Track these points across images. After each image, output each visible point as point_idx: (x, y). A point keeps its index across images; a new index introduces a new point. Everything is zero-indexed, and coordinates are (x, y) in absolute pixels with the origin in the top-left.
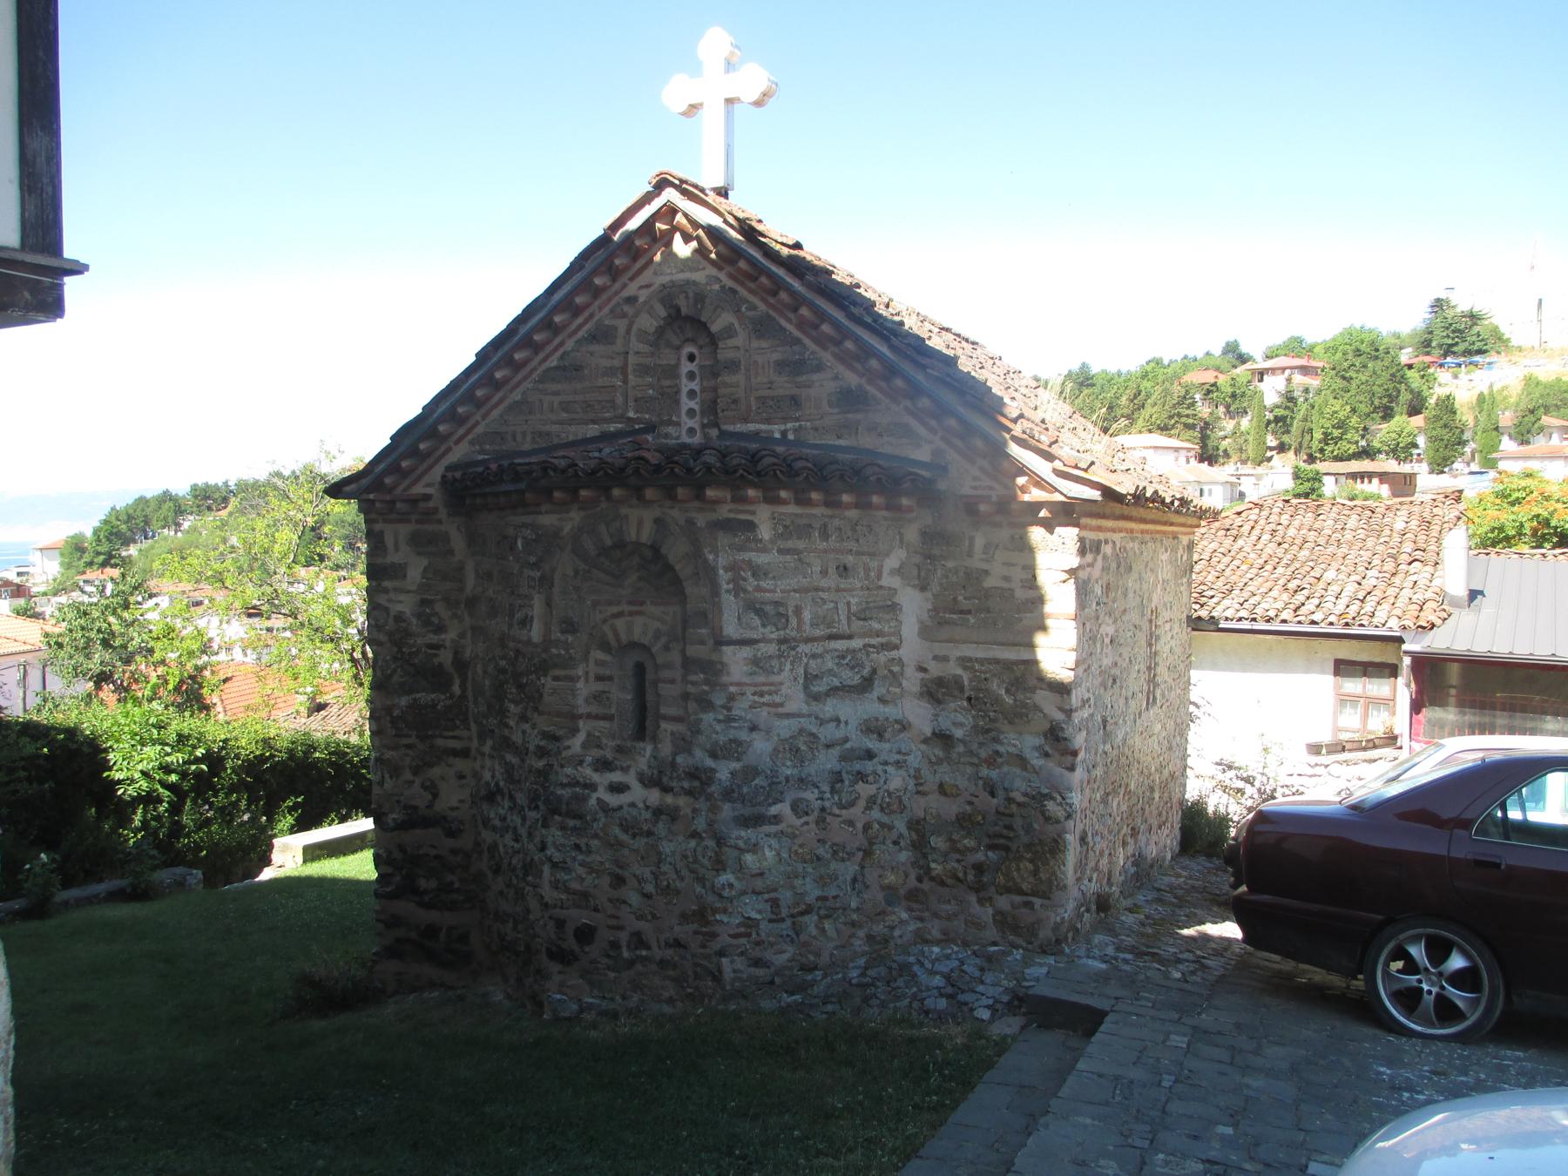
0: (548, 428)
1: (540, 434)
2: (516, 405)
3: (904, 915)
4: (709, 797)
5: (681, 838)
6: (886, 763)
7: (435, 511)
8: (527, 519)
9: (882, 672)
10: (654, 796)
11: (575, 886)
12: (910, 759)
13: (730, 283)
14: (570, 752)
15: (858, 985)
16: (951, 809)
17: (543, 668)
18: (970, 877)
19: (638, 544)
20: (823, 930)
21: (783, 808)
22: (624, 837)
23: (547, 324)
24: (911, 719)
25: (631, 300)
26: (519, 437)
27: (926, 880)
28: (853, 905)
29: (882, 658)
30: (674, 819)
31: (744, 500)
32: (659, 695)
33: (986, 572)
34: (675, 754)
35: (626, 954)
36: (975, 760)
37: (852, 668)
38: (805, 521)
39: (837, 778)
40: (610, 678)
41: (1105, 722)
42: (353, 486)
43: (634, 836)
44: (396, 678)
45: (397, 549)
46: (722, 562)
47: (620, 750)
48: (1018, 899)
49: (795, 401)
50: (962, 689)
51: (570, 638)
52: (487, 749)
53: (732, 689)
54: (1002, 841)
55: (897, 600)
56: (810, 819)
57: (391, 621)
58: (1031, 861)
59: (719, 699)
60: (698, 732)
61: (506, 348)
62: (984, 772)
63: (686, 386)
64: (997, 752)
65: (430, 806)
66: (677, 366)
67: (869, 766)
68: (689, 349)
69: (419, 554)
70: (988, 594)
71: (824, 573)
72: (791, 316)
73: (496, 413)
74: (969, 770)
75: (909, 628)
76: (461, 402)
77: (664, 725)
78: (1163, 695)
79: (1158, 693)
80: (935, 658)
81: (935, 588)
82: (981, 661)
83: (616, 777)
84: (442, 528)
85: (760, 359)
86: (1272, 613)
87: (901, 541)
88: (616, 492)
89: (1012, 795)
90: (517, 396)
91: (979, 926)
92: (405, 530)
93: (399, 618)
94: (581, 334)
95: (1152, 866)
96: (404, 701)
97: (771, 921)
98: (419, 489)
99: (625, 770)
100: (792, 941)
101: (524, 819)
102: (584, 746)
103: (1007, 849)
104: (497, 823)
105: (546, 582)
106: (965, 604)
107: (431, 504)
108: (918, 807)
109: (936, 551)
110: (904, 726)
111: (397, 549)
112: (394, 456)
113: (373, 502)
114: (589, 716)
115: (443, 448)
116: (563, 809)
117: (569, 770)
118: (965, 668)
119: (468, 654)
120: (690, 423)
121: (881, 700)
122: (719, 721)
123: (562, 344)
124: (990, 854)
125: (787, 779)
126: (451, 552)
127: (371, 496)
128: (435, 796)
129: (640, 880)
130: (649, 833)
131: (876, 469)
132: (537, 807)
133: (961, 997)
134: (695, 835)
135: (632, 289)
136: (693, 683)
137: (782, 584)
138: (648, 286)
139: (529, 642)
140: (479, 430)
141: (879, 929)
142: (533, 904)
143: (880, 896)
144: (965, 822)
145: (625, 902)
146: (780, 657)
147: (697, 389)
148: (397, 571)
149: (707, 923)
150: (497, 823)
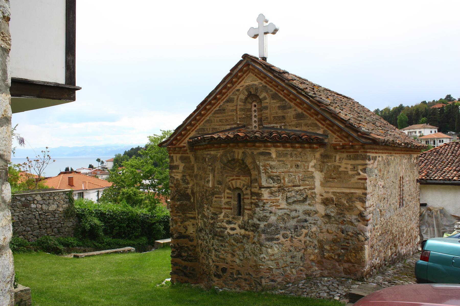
0: (216, 127)
1: (214, 129)
2: (208, 120)
3: (317, 268)
4: (258, 232)
5: (250, 244)
6: (311, 223)
8: (209, 152)
9: (309, 196)
10: (243, 231)
11: (221, 256)
12: (318, 222)
13: (265, 84)
14: (220, 218)
15: (301, 288)
16: (330, 237)
17: (213, 194)
18: (336, 258)
19: (238, 159)
20: (292, 272)
21: (280, 236)
22: (234, 243)
23: (215, 98)
24: (318, 210)
25: (238, 90)
26: (208, 130)
29: (309, 192)
30: (248, 238)
31: (267, 147)
32: (244, 203)
33: (340, 166)
34: (248, 220)
35: (235, 277)
36: (338, 223)
37: (300, 195)
38: (286, 152)
39: (296, 227)
40: (231, 198)
42: (165, 144)
43: (237, 243)
44: (176, 197)
45: (177, 161)
46: (261, 164)
47: (233, 218)
48: (350, 265)
49: (284, 117)
50: (333, 201)
51: (220, 186)
52: (199, 217)
53: (265, 201)
55: (313, 175)
56: (288, 239)
57: (175, 181)
58: (354, 253)
59: (261, 204)
60: (255, 213)
61: (204, 105)
62: (340, 226)
63: (254, 114)
64: (344, 220)
66: (251, 108)
67: (305, 224)
68: (254, 103)
71: (291, 167)
72: (282, 93)
73: (202, 123)
74: (336, 226)
75: (318, 183)
76: (192, 120)
77: (246, 211)
78: (407, 203)
79: (404, 202)
80: (325, 192)
81: (325, 171)
82: (339, 193)
83: (232, 226)
84: (188, 155)
85: (274, 106)
86: (450, 178)
87: (315, 158)
88: (231, 144)
89: (349, 233)
90: (208, 118)
91: (339, 272)
92: (179, 155)
94: (224, 100)
95: (404, 256)
96: (178, 203)
97: (276, 269)
98: (182, 144)
99: (235, 224)
100: (283, 275)
101: (208, 237)
102: (224, 217)
103: (347, 249)
104: (202, 238)
105: (213, 170)
106: (334, 176)
107: (185, 149)
108: (321, 237)
109: (325, 161)
110: (316, 212)
111: (177, 161)
112: (175, 135)
114: (225, 208)
115: (189, 133)
116: (218, 235)
117: (219, 224)
118: (334, 195)
120: (255, 125)
121: (309, 204)
122: (261, 210)
123: (220, 103)
124: (342, 251)
125: (281, 227)
126: (191, 162)
128: (187, 230)
130: (242, 242)
131: (306, 136)
133: (331, 293)
134: (254, 243)
135: (238, 87)
136: (254, 199)
138: (242, 86)
139: (209, 187)
140: (198, 128)
141: (309, 272)
144: (335, 241)
145: (235, 262)
146: (279, 192)
147: (257, 115)
150: (202, 238)
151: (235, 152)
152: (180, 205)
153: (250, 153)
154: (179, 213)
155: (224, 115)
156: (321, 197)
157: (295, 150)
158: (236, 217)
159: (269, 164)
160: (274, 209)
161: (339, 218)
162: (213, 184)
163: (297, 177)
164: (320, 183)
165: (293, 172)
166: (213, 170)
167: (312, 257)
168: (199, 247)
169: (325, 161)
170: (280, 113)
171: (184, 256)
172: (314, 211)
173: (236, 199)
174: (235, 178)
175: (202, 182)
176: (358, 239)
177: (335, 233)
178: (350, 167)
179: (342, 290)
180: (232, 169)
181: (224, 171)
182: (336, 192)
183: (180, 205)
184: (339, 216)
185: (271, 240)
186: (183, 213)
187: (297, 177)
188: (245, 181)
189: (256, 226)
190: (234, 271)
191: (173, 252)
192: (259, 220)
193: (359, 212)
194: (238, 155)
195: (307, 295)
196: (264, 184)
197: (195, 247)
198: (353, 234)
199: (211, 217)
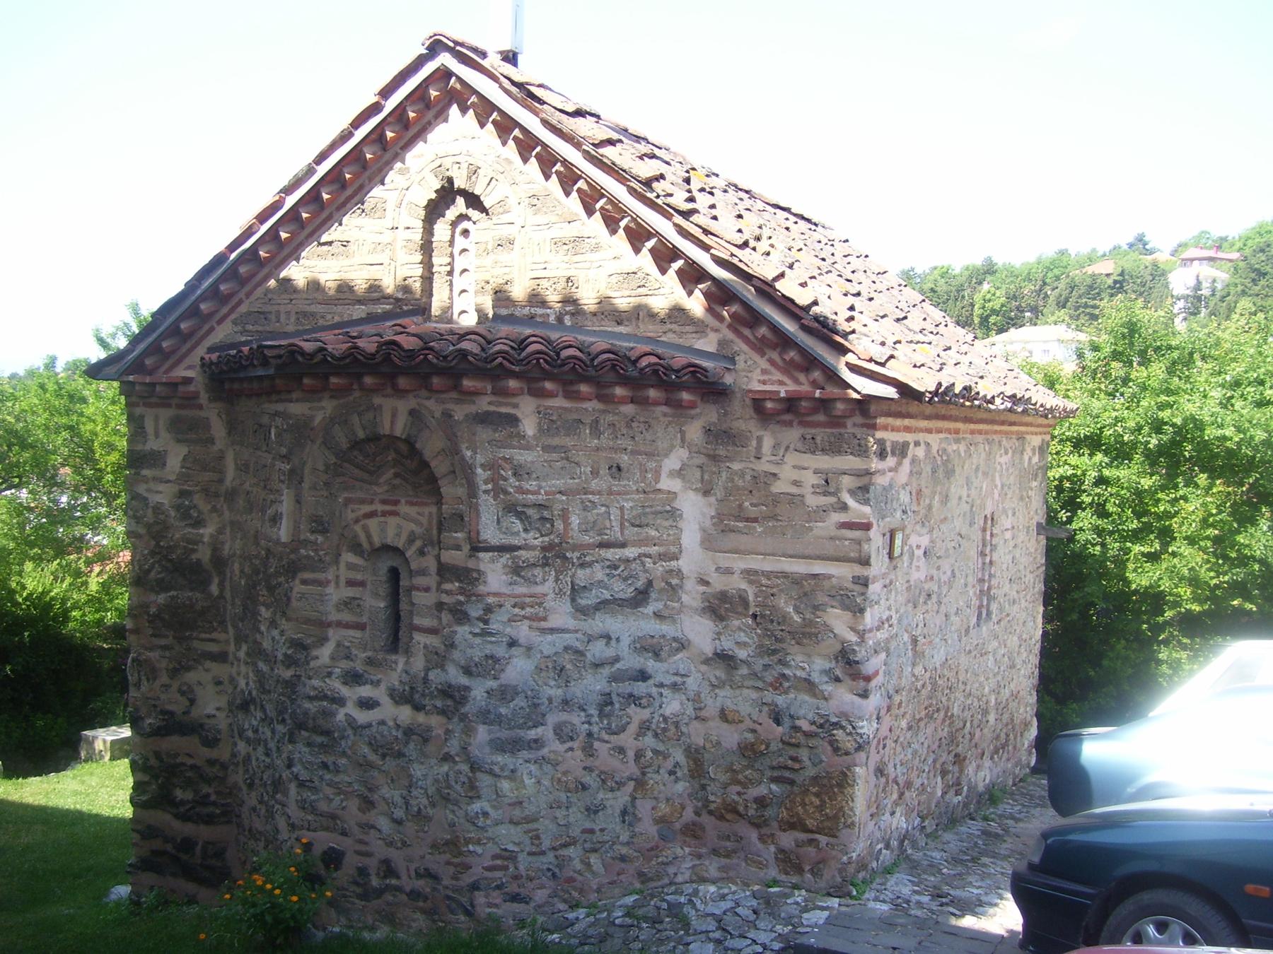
0: (313, 308)
1: (305, 314)
4: (464, 717)
5: (433, 761)
6: (661, 685)
7: (195, 396)
8: (280, 407)
9: (659, 584)
10: (405, 714)
12: (689, 681)
17: (292, 570)
19: (393, 438)
20: (588, 865)
22: (372, 757)
24: (691, 636)
27: (704, 813)
28: (624, 837)
29: (660, 568)
30: (426, 740)
32: (413, 604)
34: (427, 670)
35: (375, 882)
36: (760, 684)
37: (625, 579)
38: (575, 416)
39: (606, 701)
40: (362, 584)
41: (915, 641)
45: (157, 435)
46: (480, 459)
47: (370, 662)
50: (744, 602)
51: (320, 539)
52: (242, 654)
53: (490, 600)
54: (787, 774)
56: (575, 744)
58: (817, 795)
59: (475, 611)
60: (452, 646)
62: (769, 696)
65: (186, 713)
67: (640, 688)
69: (179, 441)
70: (776, 500)
71: (595, 473)
74: (754, 695)
75: (690, 537)
77: (419, 638)
78: (1001, 609)
81: (719, 493)
83: (365, 691)
84: (203, 414)
87: (683, 440)
88: (368, 380)
89: (798, 723)
92: (166, 414)
93: (157, 509)
96: (161, 598)
97: (530, 854)
98: (181, 372)
99: (376, 684)
101: (273, 731)
104: (250, 734)
105: (295, 477)
106: (753, 511)
107: (192, 388)
109: (721, 451)
110: (682, 645)
111: (157, 435)
113: (132, 383)
114: (339, 624)
115: (206, 327)
116: (317, 729)
117: (316, 682)
118: (751, 582)
119: (226, 551)
121: (657, 615)
122: (475, 635)
124: (773, 787)
126: (211, 441)
127: (131, 378)
128: (192, 702)
129: (389, 803)
130: (400, 755)
132: (283, 721)
133: (730, 943)
134: (447, 758)
136: (448, 593)
137: (547, 485)
139: (278, 542)
142: (282, 823)
143: (652, 830)
144: (750, 751)
145: (373, 827)
148: (157, 459)
149: (460, 854)
150: (250, 734)
151: (380, 406)
153: (438, 415)
154: (166, 637)
156: (702, 588)
157: (610, 407)
160: (523, 631)
161: (766, 667)
162: (296, 528)
163: (615, 513)
164: (698, 537)
165: (599, 493)
166: (295, 477)
169: (721, 451)
171: (182, 803)
172: (675, 639)
173: (383, 590)
174: (380, 508)
177: (748, 723)
178: (811, 479)
180: (371, 473)
184: (766, 660)
185: (512, 746)
187: (615, 513)
189: (454, 697)
190: (372, 863)
192: (467, 671)
193: (839, 647)
194: (392, 423)
196: (490, 534)
197: (224, 767)
198: (813, 728)
199: (285, 655)
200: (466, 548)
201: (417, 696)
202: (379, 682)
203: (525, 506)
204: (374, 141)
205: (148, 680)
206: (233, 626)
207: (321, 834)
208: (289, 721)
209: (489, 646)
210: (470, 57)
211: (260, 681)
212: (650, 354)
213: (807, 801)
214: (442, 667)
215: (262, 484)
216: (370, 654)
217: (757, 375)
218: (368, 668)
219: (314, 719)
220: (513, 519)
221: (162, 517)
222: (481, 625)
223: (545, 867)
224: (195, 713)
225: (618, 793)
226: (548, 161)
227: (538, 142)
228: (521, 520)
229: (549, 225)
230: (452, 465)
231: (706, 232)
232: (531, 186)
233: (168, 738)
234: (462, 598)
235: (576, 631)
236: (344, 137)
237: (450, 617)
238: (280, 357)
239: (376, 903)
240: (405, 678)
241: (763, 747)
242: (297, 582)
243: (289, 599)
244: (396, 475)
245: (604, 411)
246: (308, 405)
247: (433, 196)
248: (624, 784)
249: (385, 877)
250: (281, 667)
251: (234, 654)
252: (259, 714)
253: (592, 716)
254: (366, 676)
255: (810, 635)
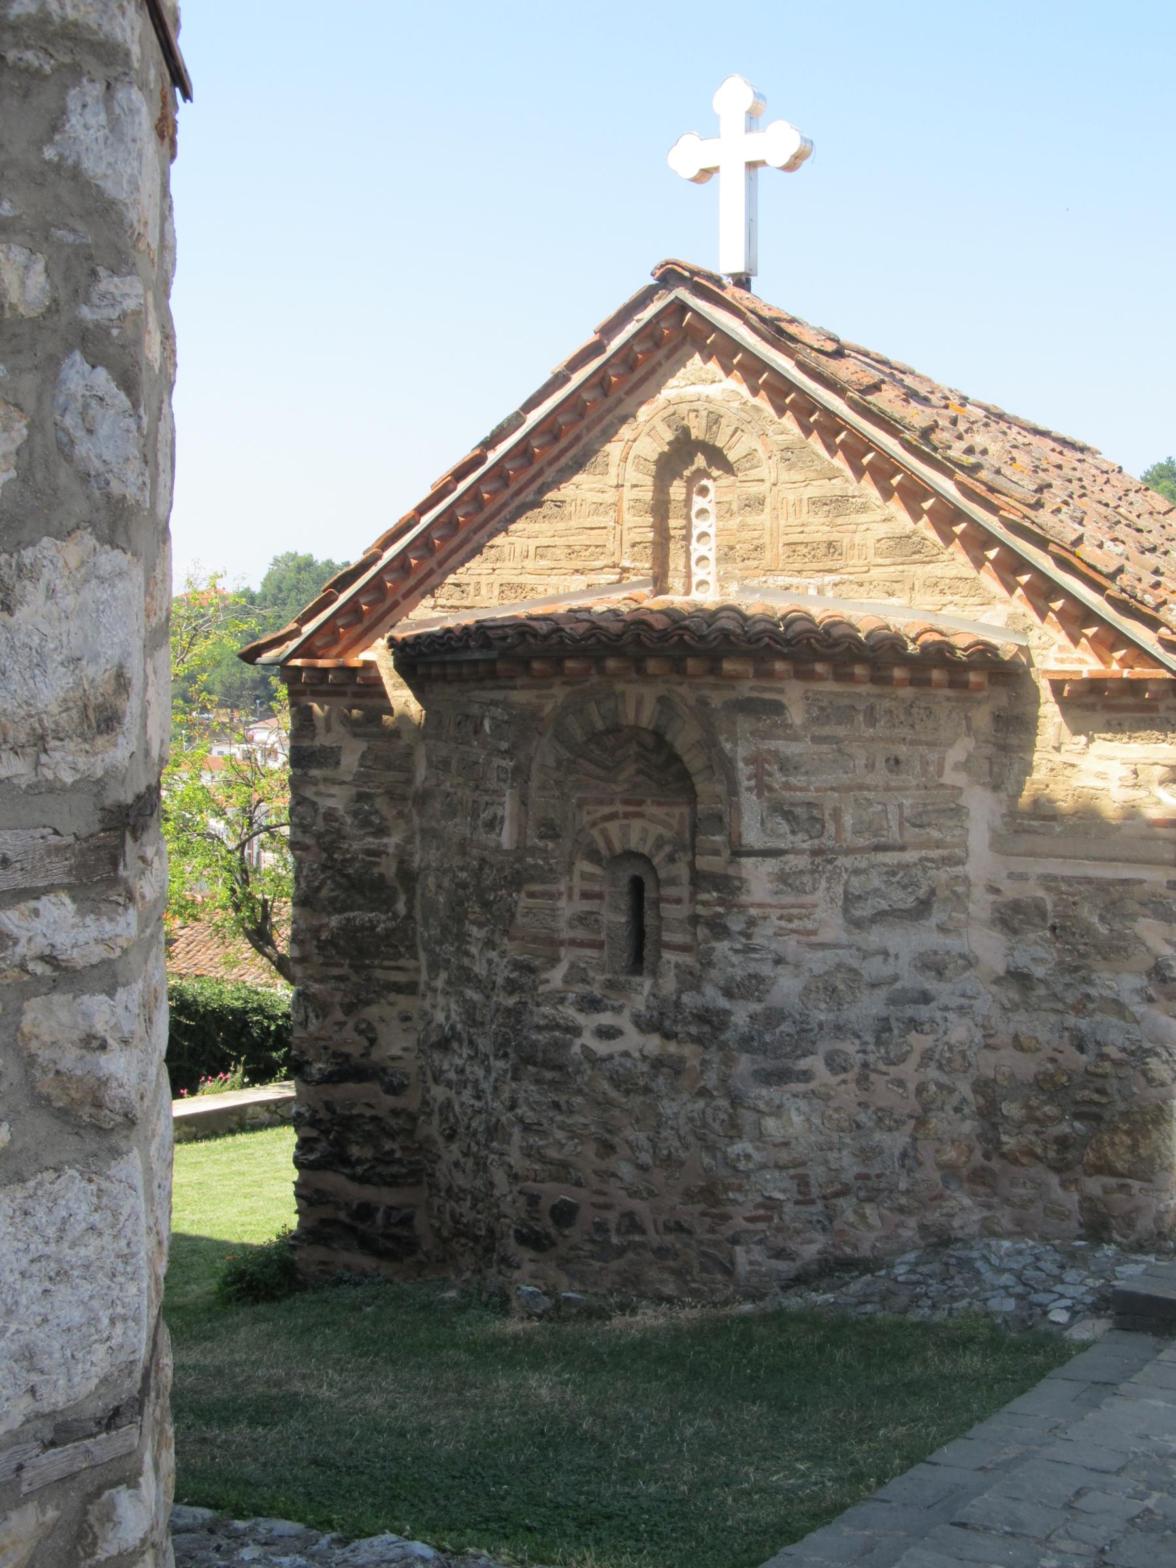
3: (967, 1202)
4: (722, 1046)
5: (685, 1096)
6: (946, 1009)
8: (498, 695)
9: (942, 893)
10: (653, 1044)
11: (552, 1153)
12: (977, 1003)
15: (906, 1283)
16: (1027, 1067)
17: (517, 881)
18: (1051, 1154)
19: (636, 728)
20: (863, 1217)
21: (814, 1062)
22: (613, 1094)
26: (484, 591)
27: (995, 1158)
28: (902, 1186)
30: (678, 1073)
31: (771, 675)
32: (660, 918)
34: (680, 992)
36: (1060, 1006)
37: (905, 887)
38: (847, 702)
39: (884, 1026)
40: (599, 896)
43: (627, 1092)
44: (325, 893)
46: (742, 752)
47: (610, 985)
48: (1112, 1181)
50: (1043, 915)
51: (551, 845)
52: (439, 983)
53: (753, 911)
55: (962, 801)
57: (320, 821)
58: (1128, 1133)
59: (736, 924)
60: (710, 964)
62: (1071, 1020)
64: (1088, 996)
67: (924, 1012)
69: (355, 735)
71: (870, 767)
74: (1053, 1018)
77: (667, 955)
80: (1011, 875)
83: (606, 1019)
87: (969, 728)
89: (1106, 1050)
93: (330, 815)
96: (334, 921)
97: (797, 1203)
99: (618, 1010)
101: (488, 1070)
102: (567, 981)
103: (1098, 1118)
104: (452, 1075)
105: (520, 774)
108: (986, 1064)
110: (970, 962)
111: (328, 729)
114: (573, 943)
116: (543, 1061)
117: (546, 1010)
118: (1048, 889)
121: (942, 928)
122: (736, 951)
124: (1077, 1124)
125: (821, 1026)
128: (373, 1041)
129: (633, 1147)
130: (647, 1090)
132: (506, 1055)
134: (704, 1093)
136: (705, 904)
139: (498, 849)
142: (499, 1176)
144: (1048, 1085)
145: (614, 1175)
146: (813, 872)
148: (328, 757)
150: (452, 1075)
151: (623, 694)
152: (342, 929)
153: (692, 702)
154: (342, 965)
155: (561, 526)
156: (992, 897)
157: (887, 690)
158: (622, 978)
159: (776, 753)
160: (790, 946)
161: (1068, 986)
162: (522, 833)
163: (892, 811)
164: (987, 837)
165: (876, 788)
166: (520, 774)
167: (950, 1154)
168: (436, 1119)
170: (818, 528)
171: (359, 1161)
173: (624, 903)
174: (620, 808)
175: (457, 828)
176: (1144, 1073)
177: (1048, 1051)
179: (1079, 1284)
180: (606, 768)
181: (571, 778)
182: (1054, 878)
183: (348, 930)
184: (1067, 979)
185: (780, 1077)
186: (357, 969)
187: (892, 811)
188: (664, 823)
189: (711, 1022)
190: (612, 1217)
191: (304, 1145)
192: (728, 993)
193: (1152, 962)
194: (638, 711)
195: (934, 1307)
196: (752, 836)
197: (413, 1118)
198: (1123, 1056)
199: (508, 979)
200: (726, 853)
201: (667, 1023)
202: (621, 1007)
203: (792, 804)
204: (594, 387)
205: (317, 1017)
206: (425, 950)
207: (549, 1186)
208: (512, 1055)
209: (753, 965)
210: (706, 286)
211: (467, 1012)
212: (932, 630)
213: (1117, 1140)
214: (697, 988)
215: (472, 784)
216: (609, 976)
217: (1053, 652)
218: (608, 992)
219: (544, 1052)
220: (779, 819)
221: (336, 825)
222: (743, 940)
223: (815, 1218)
224: (376, 1055)
225: (896, 1134)
226: (805, 408)
227: (792, 387)
228: (788, 821)
229: (807, 482)
230: (709, 759)
231: (992, 490)
232: (783, 437)
233: (342, 1085)
234: (720, 910)
235: (850, 947)
236: (559, 380)
237: (706, 931)
238: (504, 638)
239: (616, 1264)
240: (653, 1002)
241: (1064, 1079)
242: (523, 895)
243: (513, 915)
244: (639, 772)
245: (880, 696)
246: (536, 692)
247: (666, 448)
248: (904, 1123)
249: (628, 1232)
250: (502, 994)
251: (427, 984)
252: (466, 1051)
253: (866, 1043)
254: (606, 1001)
255: (1118, 950)
